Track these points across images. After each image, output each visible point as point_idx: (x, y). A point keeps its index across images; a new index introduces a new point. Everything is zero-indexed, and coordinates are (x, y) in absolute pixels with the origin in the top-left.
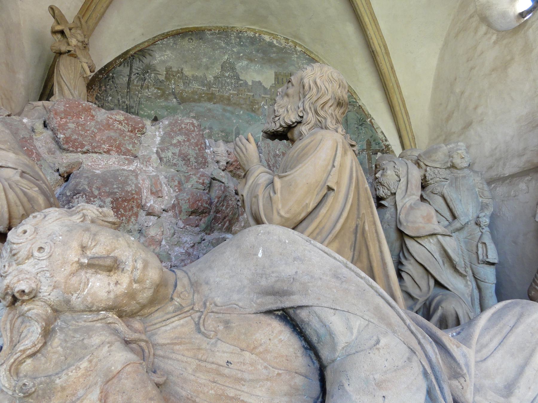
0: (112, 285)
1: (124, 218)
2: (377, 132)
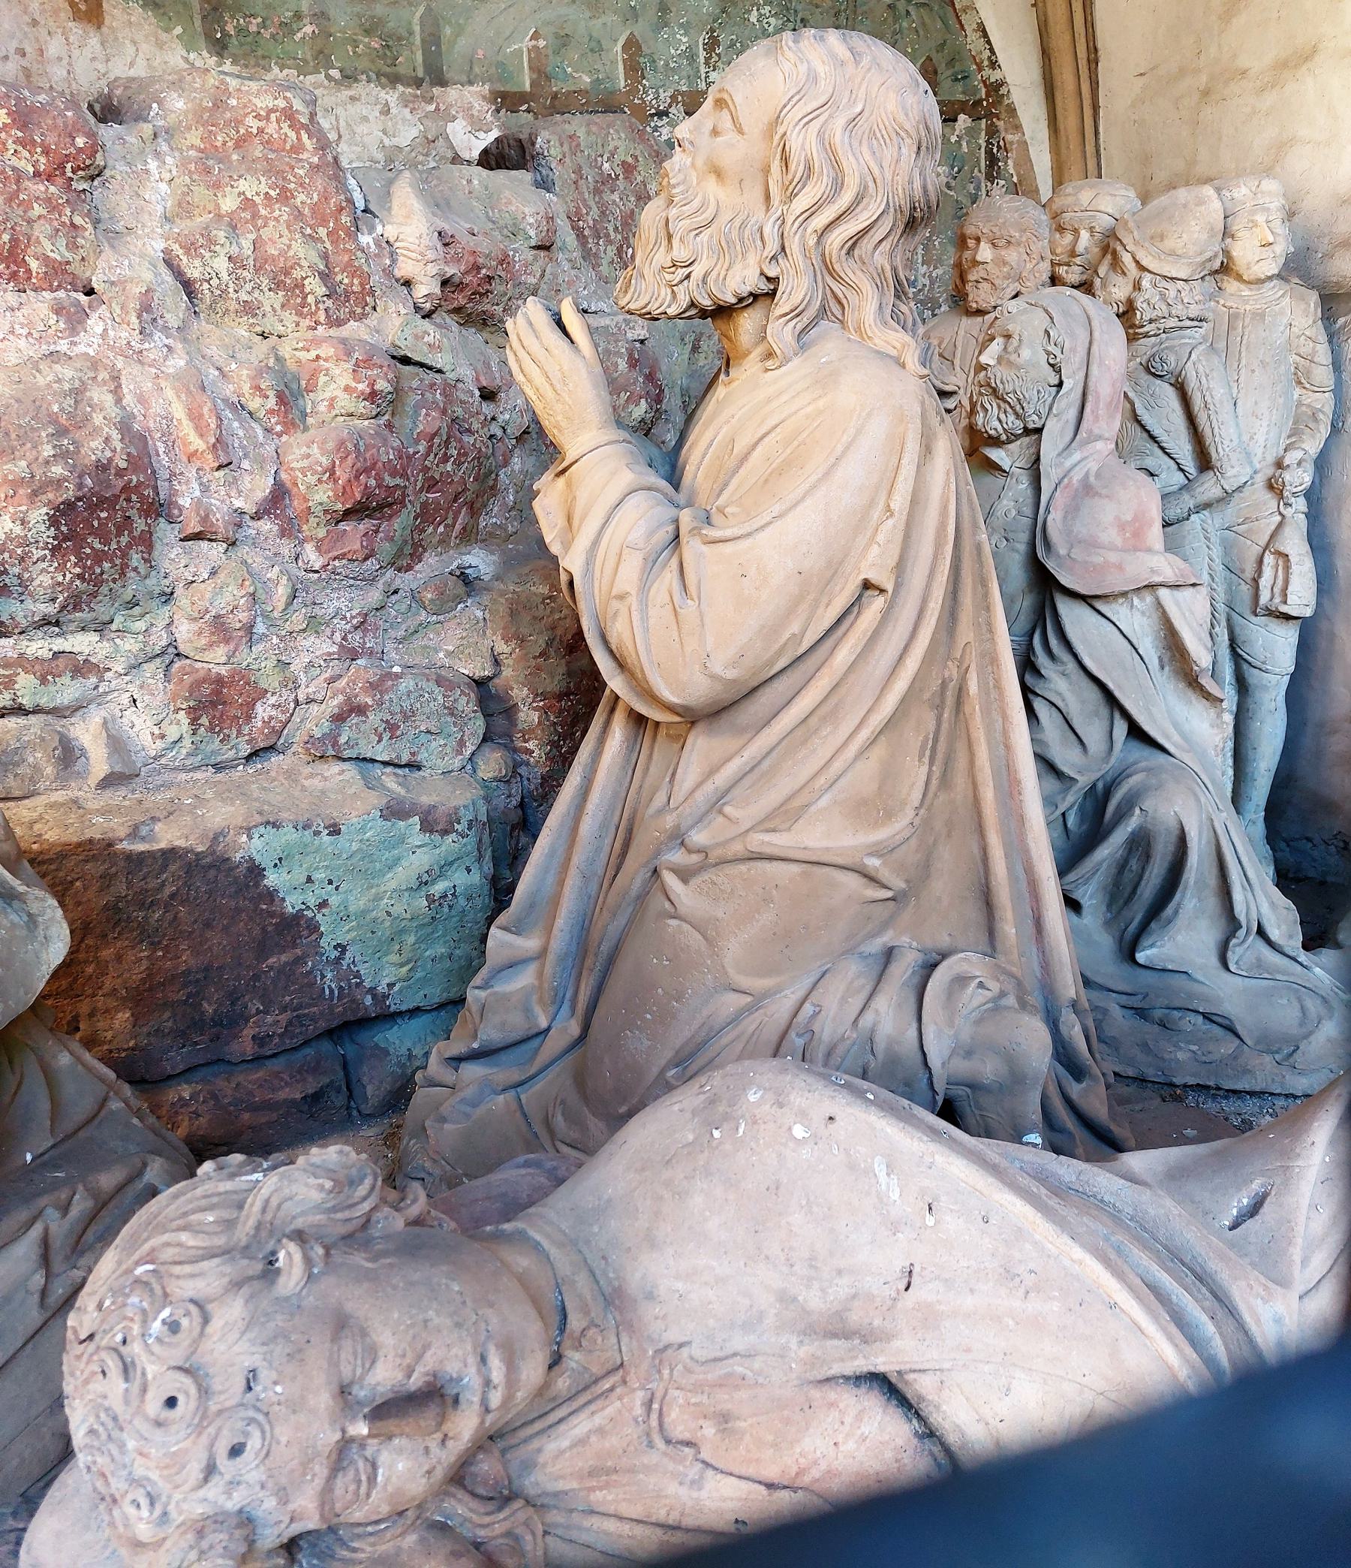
1: (106, 565)
2: (962, 26)
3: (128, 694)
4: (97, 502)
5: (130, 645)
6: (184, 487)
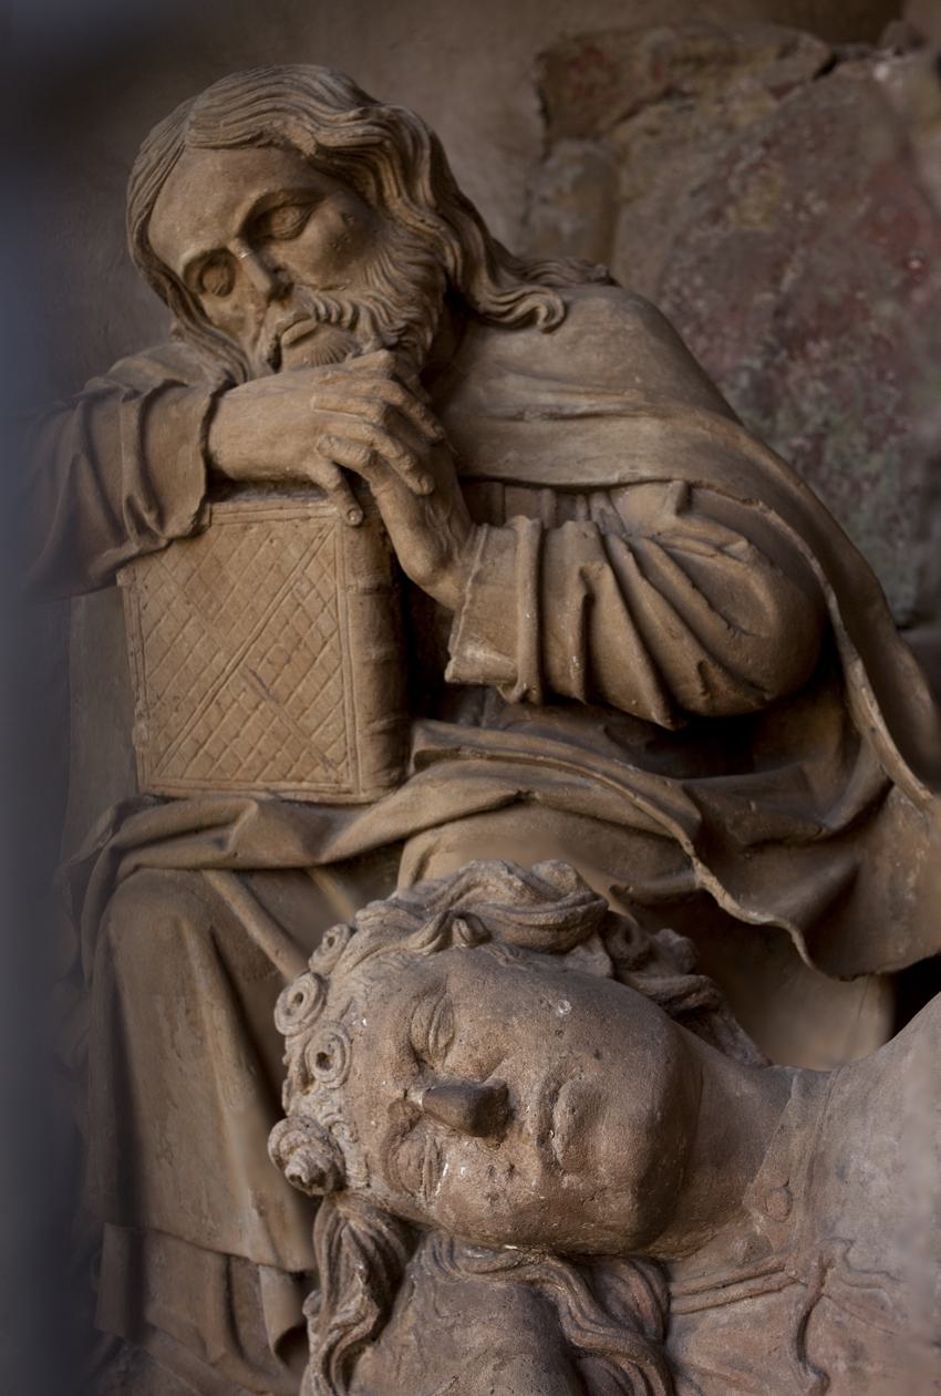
0: (500, 1175)
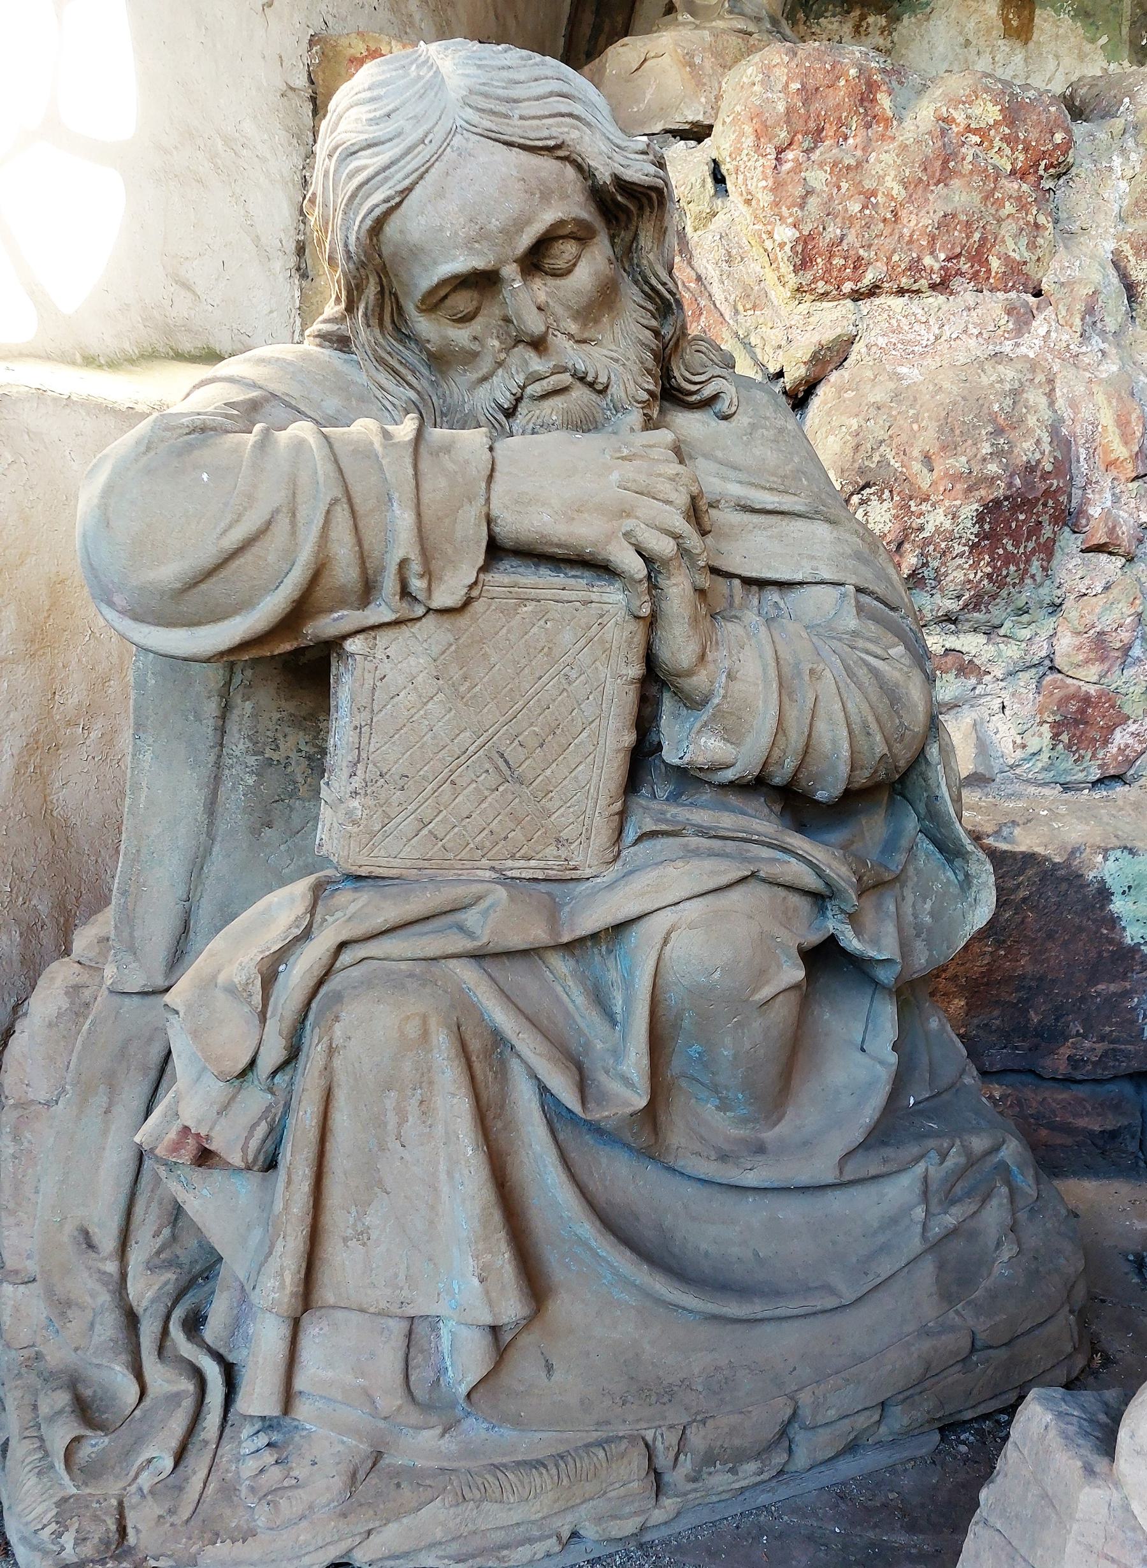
3: (1000, 700)
4: (1021, 502)
5: (1012, 651)
6: (1097, 496)
